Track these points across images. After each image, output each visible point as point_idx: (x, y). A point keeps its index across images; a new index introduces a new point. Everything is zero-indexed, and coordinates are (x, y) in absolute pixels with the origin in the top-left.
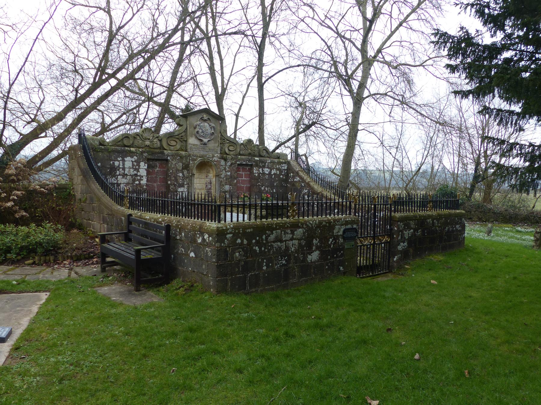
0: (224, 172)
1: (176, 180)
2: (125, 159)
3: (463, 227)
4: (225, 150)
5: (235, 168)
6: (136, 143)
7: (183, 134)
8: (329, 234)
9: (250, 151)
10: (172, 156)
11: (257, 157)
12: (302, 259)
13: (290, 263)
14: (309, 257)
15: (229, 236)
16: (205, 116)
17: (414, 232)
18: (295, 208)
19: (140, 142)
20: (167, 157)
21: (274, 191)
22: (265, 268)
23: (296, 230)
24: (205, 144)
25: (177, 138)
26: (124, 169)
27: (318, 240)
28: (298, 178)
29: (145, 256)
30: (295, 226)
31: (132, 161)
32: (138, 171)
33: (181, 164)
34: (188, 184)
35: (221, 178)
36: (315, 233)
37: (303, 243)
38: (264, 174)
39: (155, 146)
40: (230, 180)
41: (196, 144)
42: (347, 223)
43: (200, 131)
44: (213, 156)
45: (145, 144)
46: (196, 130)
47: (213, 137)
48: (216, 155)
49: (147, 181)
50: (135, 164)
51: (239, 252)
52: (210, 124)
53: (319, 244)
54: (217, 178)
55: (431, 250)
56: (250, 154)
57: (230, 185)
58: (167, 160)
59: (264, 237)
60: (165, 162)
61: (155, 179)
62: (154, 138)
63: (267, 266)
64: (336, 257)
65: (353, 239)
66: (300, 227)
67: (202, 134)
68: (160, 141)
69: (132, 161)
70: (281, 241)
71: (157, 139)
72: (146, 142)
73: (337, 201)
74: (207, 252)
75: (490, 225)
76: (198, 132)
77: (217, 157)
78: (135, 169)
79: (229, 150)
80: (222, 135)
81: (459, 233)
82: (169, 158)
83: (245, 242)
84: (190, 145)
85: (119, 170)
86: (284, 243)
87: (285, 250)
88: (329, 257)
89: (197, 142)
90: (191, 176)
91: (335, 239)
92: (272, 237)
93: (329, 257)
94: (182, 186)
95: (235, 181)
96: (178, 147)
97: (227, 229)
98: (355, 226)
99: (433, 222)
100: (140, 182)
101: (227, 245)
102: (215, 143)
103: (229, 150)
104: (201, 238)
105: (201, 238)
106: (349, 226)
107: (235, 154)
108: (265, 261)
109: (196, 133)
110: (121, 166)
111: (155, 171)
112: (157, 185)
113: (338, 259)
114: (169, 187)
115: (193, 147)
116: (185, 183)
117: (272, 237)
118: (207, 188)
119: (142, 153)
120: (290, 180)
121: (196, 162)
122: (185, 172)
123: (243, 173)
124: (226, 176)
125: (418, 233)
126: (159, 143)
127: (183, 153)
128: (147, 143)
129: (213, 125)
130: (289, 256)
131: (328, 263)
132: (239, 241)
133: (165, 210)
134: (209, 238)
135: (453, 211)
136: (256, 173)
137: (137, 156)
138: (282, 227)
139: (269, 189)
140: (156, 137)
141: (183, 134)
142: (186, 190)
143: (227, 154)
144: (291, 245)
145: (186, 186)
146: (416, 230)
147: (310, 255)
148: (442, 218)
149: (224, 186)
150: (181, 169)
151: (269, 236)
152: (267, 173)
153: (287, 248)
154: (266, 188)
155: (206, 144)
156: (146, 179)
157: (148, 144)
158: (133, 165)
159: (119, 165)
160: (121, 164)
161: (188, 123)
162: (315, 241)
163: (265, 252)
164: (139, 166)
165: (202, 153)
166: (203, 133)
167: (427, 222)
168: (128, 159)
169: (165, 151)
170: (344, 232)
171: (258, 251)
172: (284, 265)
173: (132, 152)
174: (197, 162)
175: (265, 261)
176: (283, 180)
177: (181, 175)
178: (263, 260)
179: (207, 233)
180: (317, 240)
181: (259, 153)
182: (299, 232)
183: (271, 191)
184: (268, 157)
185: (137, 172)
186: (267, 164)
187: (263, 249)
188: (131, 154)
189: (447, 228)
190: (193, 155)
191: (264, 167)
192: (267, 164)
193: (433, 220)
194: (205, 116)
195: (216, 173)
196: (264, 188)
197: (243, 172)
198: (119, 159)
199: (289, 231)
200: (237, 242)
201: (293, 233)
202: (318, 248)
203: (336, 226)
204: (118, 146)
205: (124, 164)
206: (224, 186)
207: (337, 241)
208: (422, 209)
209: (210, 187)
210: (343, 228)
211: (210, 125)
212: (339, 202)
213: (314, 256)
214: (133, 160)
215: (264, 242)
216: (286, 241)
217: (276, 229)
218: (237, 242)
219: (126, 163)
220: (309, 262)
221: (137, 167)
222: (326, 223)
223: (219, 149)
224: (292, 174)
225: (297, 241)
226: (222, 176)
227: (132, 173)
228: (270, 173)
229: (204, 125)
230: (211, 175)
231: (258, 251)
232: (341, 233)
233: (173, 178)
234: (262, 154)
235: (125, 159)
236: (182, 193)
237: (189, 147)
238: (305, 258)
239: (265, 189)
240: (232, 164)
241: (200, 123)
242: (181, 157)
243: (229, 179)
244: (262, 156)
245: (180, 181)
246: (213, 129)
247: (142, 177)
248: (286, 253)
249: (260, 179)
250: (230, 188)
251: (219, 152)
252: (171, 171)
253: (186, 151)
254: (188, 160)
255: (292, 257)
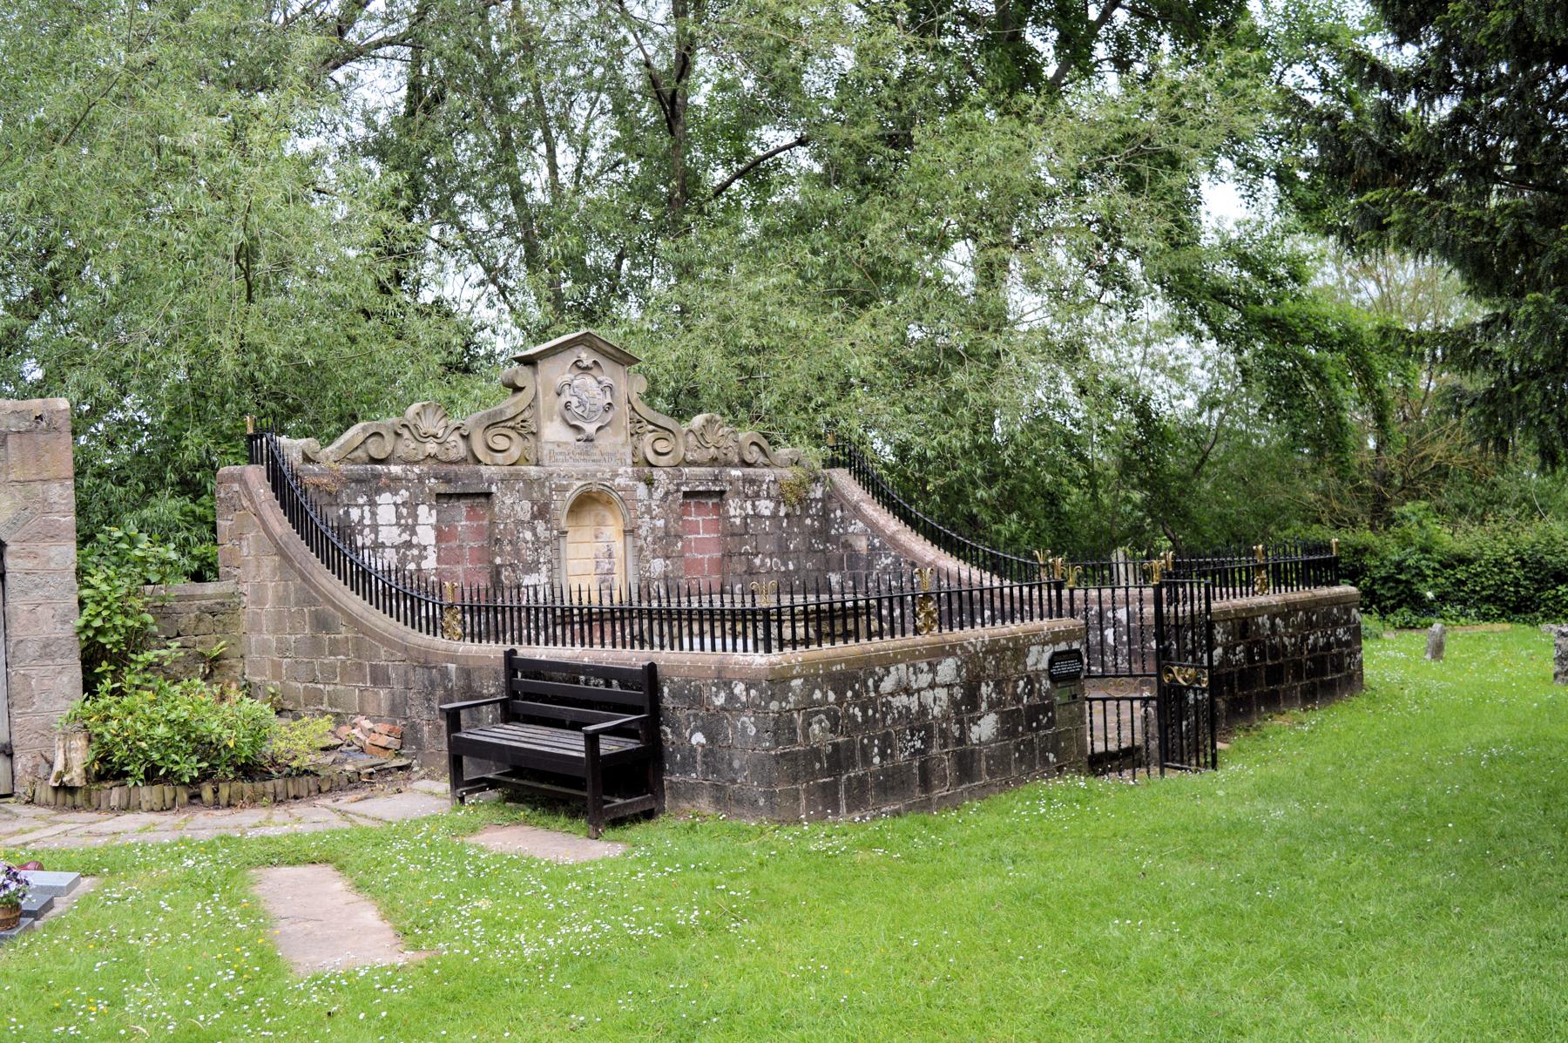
0: (647, 517)
1: (517, 552)
2: (377, 498)
3: (1357, 634)
4: (644, 453)
5: (675, 506)
6: (401, 450)
7: (526, 415)
8: (1016, 669)
9: (712, 449)
10: (502, 481)
11: (735, 466)
12: (957, 734)
13: (932, 747)
14: (974, 728)
15: (796, 683)
16: (584, 355)
17: (1226, 652)
18: (931, 606)
19: (413, 445)
20: (489, 486)
21: (791, 567)
22: (877, 760)
23: (939, 663)
24: (589, 440)
25: (513, 428)
26: (375, 528)
27: (991, 684)
28: (860, 525)
29: (608, 746)
30: (937, 653)
31: (395, 504)
32: (413, 533)
33: (527, 505)
34: (550, 561)
35: (639, 537)
36: (983, 669)
37: (958, 692)
38: (757, 516)
39: (453, 455)
40: (666, 541)
41: (564, 440)
42: (1056, 638)
43: (575, 401)
44: (615, 475)
45: (424, 452)
46: (563, 399)
47: (610, 415)
48: (621, 471)
49: (439, 560)
50: (404, 511)
51: (820, 722)
52: (600, 378)
53: (994, 695)
54: (629, 539)
55: (1273, 701)
56: (714, 461)
57: (667, 557)
58: (488, 495)
59: (870, 682)
60: (483, 500)
61: (458, 552)
62: (448, 431)
63: (883, 755)
64: (1037, 729)
65: (1073, 677)
66: (949, 655)
67: (579, 411)
68: (465, 438)
69: (395, 504)
70: (908, 691)
71: (456, 433)
72: (428, 446)
73: (986, 584)
74: (744, 728)
75: (1437, 626)
76: (567, 406)
77: (625, 477)
78: (405, 528)
79: (657, 453)
80: (633, 409)
81: (1346, 651)
82: (494, 489)
83: (832, 697)
84: (550, 447)
85: (361, 532)
86: (916, 695)
87: (917, 712)
88: (1020, 729)
89: (569, 436)
90: (557, 538)
91: (1030, 682)
92: (887, 685)
93: (1020, 729)
94: (533, 568)
95: (680, 544)
96: (515, 453)
97: (792, 667)
98: (1076, 646)
99: (1273, 624)
100: (418, 565)
101: (792, 706)
102: (616, 434)
103: (657, 453)
104: (723, 694)
105: (723, 694)
106: (1063, 646)
107: (672, 463)
108: (876, 742)
109: (563, 407)
110: (367, 521)
111: (456, 528)
112: (465, 571)
113: (1042, 733)
114: (499, 573)
115: (557, 450)
116: (542, 560)
117: (887, 685)
118: (599, 571)
119: (420, 478)
120: (833, 532)
121: (568, 495)
122: (540, 526)
123: (700, 519)
124: (653, 529)
125: (1235, 655)
126: (461, 444)
127: (533, 471)
128: (431, 447)
129: (607, 380)
130: (928, 729)
131: (1019, 745)
132: (818, 695)
133: (538, 634)
134: (747, 690)
135: (1324, 591)
136: (735, 516)
137: (407, 489)
138: (910, 656)
139: (776, 563)
140: (452, 427)
141: (526, 415)
142: (544, 580)
143: (651, 465)
144: (930, 701)
145: (544, 568)
146: (1228, 649)
147: (975, 724)
148: (1297, 611)
149: (648, 561)
150: (528, 517)
151: (881, 680)
152: (767, 513)
153: (923, 709)
154: (768, 560)
155: (592, 440)
156: (435, 555)
157: (433, 452)
158: (399, 516)
159: (362, 517)
160: (367, 514)
161: (539, 380)
162: (984, 690)
163: (876, 721)
164: (416, 517)
165: (582, 466)
166: (582, 408)
167: (1257, 624)
168: (385, 498)
169: (482, 468)
170: (1052, 662)
171: (860, 719)
172: (919, 751)
173: (397, 479)
174: (571, 495)
175: (876, 742)
176: (814, 533)
177: (528, 535)
178: (871, 739)
179: (741, 680)
180: (988, 685)
181: (740, 454)
182: (947, 669)
183: (783, 569)
184: (767, 466)
185: (411, 535)
186: (765, 487)
187: (870, 712)
188: (393, 484)
189: (1312, 637)
190: (559, 475)
191: (757, 495)
192: (765, 487)
193: (1272, 618)
194: (584, 355)
195: (626, 525)
196: (762, 561)
197: (698, 515)
198: (361, 501)
199: (925, 667)
200: (815, 697)
201: (933, 668)
202: (992, 706)
203: (1032, 648)
204: (354, 462)
205: (374, 514)
206: (648, 561)
207: (1037, 686)
208: (733, 628)
209: (607, 566)
210: (1049, 651)
211: (600, 383)
212: (991, 590)
213: (985, 728)
214: (399, 501)
215: (872, 694)
216: (919, 691)
217: (896, 662)
218: (815, 697)
219: (380, 510)
220: (975, 742)
221: (410, 521)
222: (1008, 640)
223: (629, 450)
224: (839, 513)
225: (946, 690)
226: (643, 532)
227: (398, 541)
228: (774, 516)
229: (584, 384)
230: (612, 531)
231: (860, 719)
232: (1044, 665)
233: (509, 548)
234: (748, 458)
235: (377, 498)
236: (535, 590)
237: (545, 451)
238: (964, 733)
239: (763, 564)
240: (667, 493)
241: (572, 376)
242: (529, 483)
243: (661, 539)
244: (749, 465)
245: (529, 556)
246: (608, 393)
247: (425, 548)
248: (919, 723)
249: (747, 533)
250: (666, 566)
251: (629, 461)
252: (502, 527)
253: (537, 465)
254: (547, 491)
255: (936, 731)
